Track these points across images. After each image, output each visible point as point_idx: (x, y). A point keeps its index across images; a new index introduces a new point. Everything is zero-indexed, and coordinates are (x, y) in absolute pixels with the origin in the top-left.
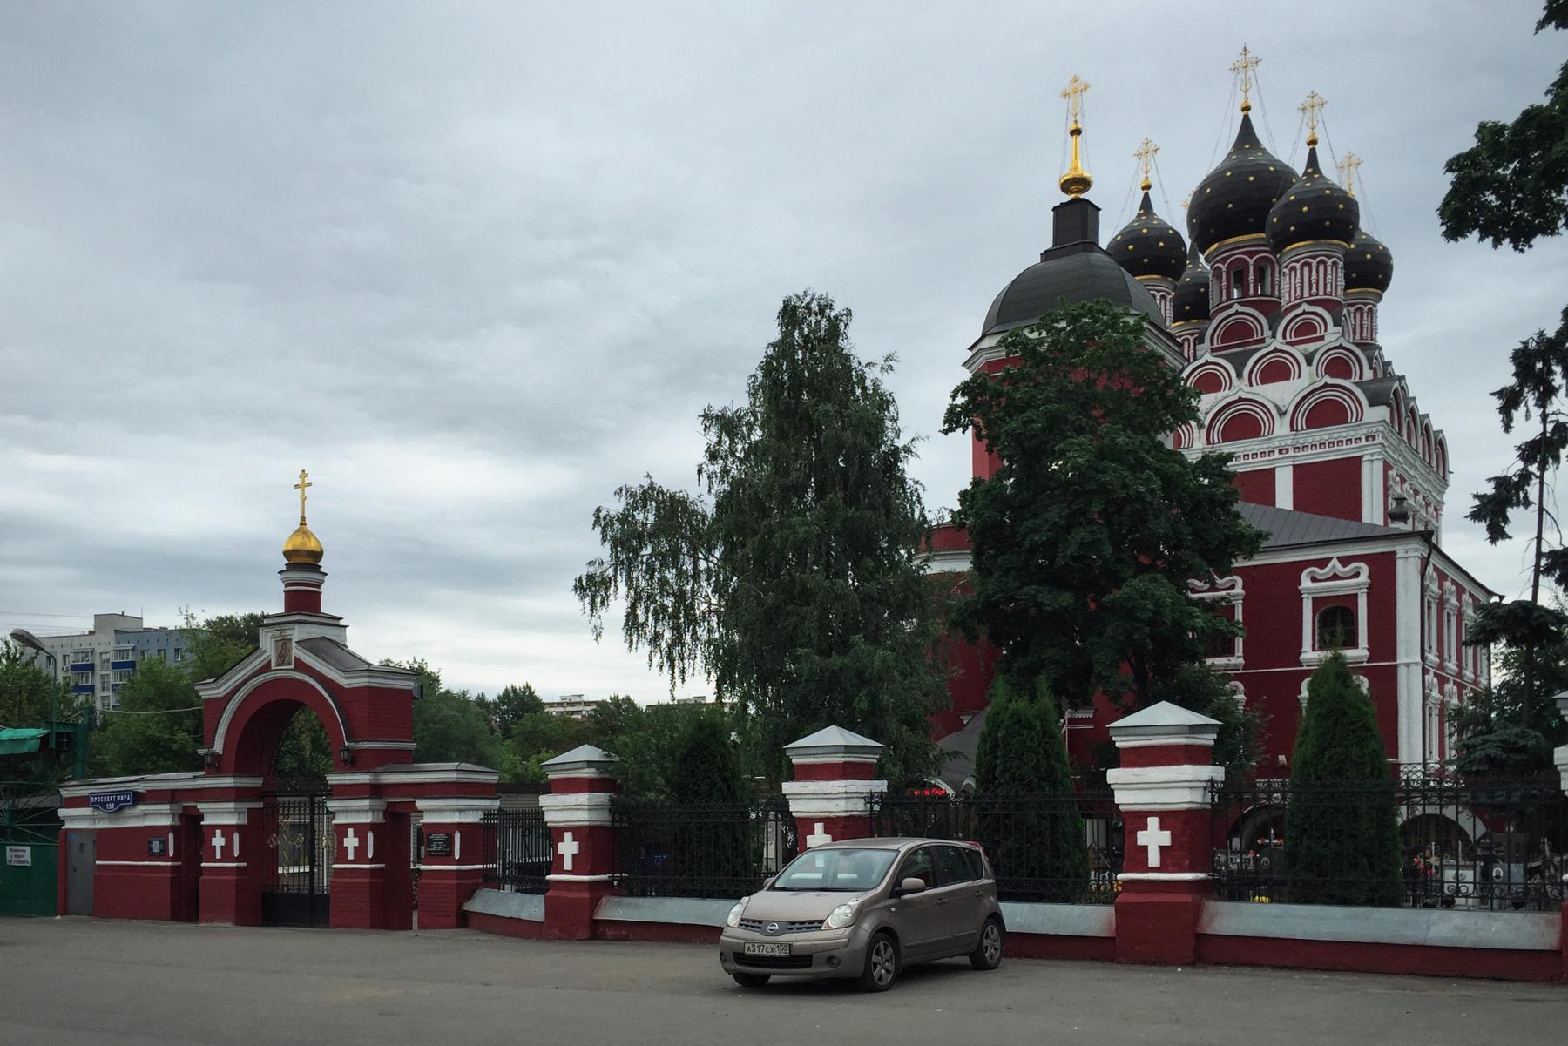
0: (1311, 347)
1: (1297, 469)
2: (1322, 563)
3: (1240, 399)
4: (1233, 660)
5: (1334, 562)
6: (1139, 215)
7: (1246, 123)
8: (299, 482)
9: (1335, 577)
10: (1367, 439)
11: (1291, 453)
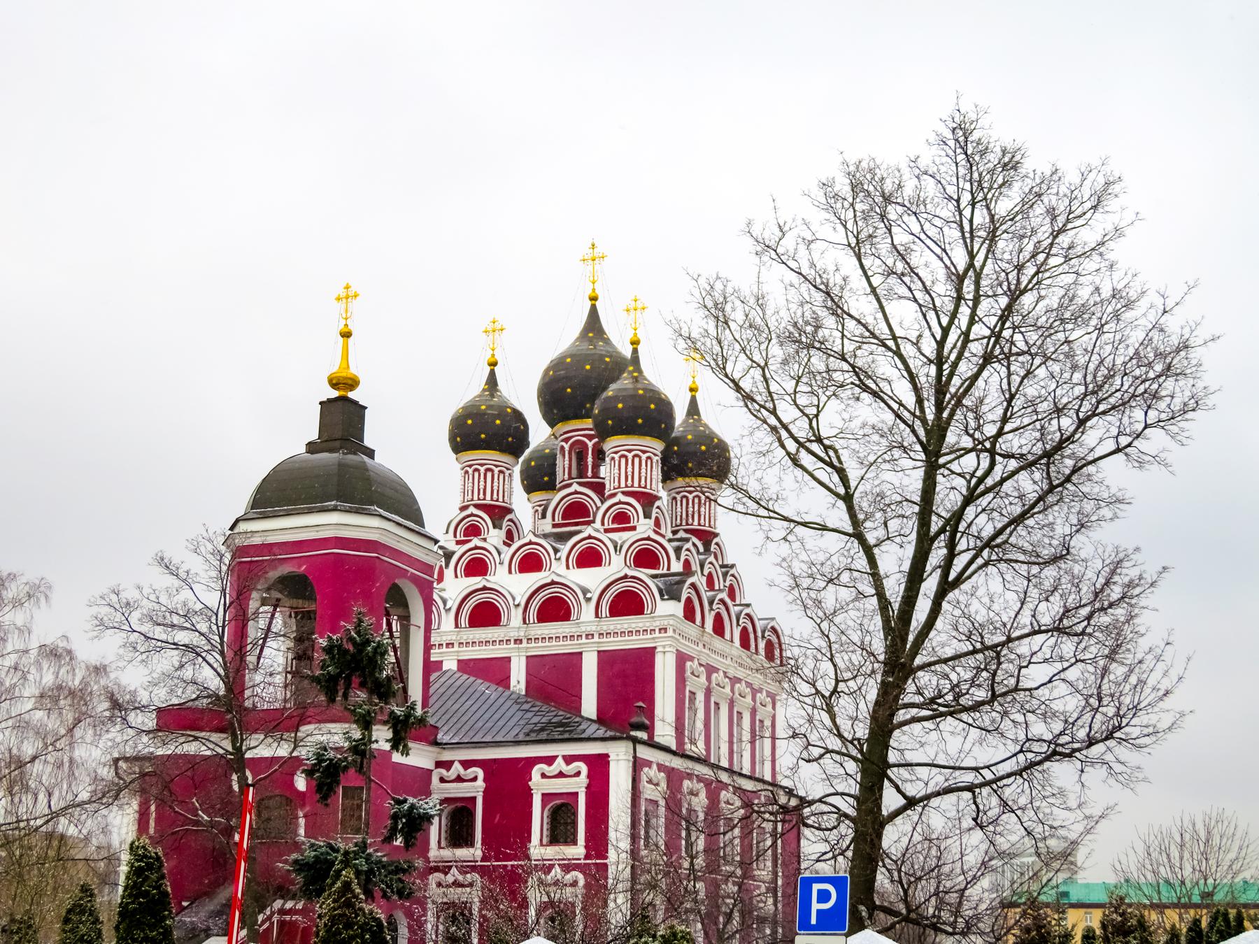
1: (600, 653)
2: (550, 760)
3: (553, 583)
5: (560, 761)
6: (484, 390)
7: (594, 313)
8: (343, 293)
9: (561, 775)
11: (596, 639)
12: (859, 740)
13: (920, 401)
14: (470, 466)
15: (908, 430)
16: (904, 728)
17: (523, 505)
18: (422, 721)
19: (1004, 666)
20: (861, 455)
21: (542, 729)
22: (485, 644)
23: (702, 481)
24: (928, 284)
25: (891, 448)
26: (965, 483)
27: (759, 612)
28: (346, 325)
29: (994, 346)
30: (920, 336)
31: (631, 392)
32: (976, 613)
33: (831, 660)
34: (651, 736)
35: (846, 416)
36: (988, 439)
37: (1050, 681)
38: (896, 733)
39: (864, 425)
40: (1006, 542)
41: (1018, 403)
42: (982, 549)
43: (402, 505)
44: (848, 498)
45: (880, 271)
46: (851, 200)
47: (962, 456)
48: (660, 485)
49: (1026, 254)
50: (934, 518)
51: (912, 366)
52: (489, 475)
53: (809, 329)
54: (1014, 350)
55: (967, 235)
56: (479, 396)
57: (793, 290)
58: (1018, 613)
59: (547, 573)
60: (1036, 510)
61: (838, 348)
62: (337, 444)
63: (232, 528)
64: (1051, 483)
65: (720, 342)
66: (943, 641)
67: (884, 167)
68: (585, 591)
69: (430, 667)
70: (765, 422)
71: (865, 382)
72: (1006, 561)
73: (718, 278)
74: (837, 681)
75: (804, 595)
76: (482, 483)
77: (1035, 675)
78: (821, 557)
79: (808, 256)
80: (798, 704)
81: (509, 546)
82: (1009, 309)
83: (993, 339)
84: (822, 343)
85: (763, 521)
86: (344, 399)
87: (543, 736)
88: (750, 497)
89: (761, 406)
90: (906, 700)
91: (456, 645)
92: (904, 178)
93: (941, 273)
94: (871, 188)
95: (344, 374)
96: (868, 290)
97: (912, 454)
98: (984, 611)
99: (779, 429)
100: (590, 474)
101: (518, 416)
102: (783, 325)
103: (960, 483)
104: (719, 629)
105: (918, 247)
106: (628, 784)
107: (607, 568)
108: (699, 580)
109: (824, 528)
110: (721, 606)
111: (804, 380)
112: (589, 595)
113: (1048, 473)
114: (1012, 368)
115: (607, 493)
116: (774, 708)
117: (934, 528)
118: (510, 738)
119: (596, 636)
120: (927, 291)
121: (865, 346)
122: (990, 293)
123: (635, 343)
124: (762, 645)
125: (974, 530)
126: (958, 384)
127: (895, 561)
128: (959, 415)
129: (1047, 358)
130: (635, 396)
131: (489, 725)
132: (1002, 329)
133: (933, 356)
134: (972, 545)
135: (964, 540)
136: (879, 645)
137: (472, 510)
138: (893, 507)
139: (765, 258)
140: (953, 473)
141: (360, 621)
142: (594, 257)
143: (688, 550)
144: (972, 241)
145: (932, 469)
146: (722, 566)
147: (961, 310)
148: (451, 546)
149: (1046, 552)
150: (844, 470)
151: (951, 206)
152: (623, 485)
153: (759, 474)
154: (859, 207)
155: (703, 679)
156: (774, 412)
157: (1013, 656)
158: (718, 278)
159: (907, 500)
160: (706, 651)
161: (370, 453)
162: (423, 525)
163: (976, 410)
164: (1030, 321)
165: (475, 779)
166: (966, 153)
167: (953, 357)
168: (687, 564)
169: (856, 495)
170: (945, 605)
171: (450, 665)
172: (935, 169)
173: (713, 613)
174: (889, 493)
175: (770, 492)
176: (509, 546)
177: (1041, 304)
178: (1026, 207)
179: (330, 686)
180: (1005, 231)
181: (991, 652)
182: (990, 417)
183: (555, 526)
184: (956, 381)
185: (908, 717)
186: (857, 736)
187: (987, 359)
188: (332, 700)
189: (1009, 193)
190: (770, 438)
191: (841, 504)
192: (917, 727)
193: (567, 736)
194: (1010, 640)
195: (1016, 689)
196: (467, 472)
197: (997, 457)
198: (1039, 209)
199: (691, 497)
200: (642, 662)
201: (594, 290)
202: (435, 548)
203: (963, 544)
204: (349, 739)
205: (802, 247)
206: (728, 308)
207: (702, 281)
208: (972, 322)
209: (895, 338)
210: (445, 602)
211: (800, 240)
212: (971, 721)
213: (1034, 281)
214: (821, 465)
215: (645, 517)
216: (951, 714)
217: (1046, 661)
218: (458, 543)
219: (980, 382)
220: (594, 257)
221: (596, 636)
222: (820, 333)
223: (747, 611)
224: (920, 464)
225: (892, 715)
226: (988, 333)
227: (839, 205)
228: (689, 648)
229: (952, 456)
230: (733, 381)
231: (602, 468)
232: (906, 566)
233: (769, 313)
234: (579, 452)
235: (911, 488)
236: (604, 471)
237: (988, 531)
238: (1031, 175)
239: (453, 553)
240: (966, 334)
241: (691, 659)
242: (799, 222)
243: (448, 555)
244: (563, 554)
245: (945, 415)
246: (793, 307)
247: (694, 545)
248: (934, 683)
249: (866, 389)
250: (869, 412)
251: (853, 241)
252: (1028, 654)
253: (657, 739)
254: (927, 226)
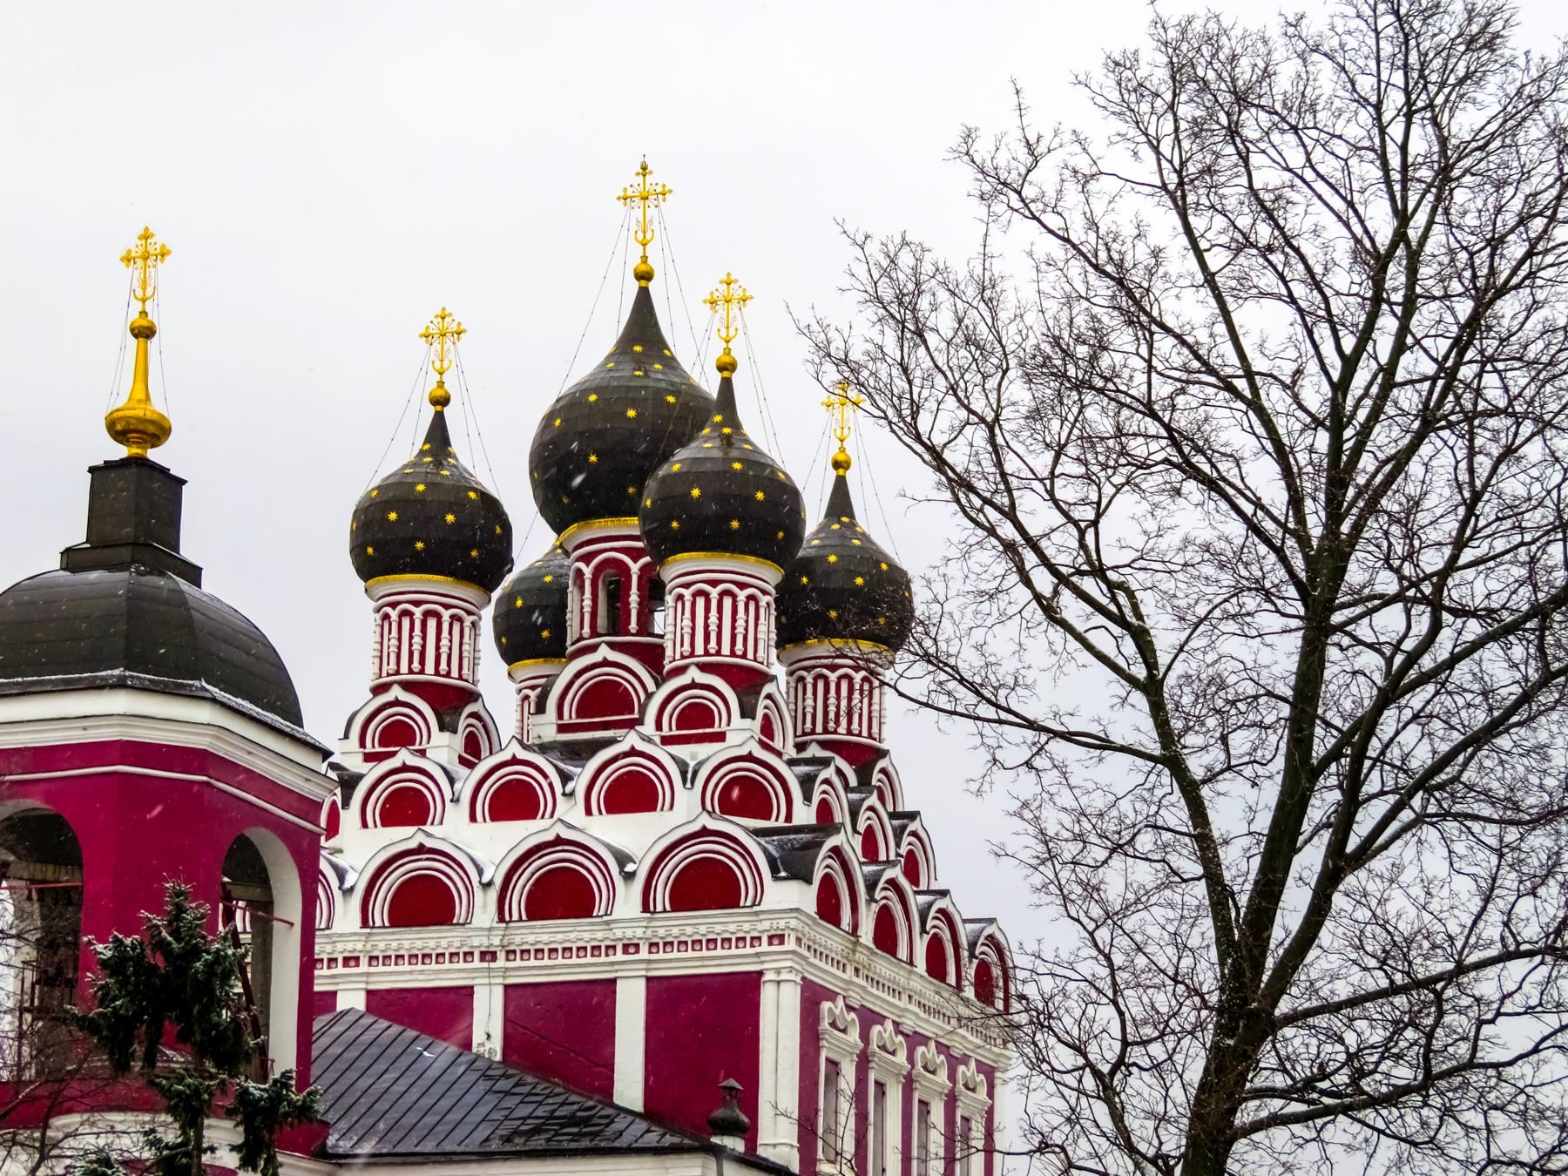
0: (703, 750)
3: (558, 841)
6: (422, 453)
7: (644, 303)
8: (136, 247)
10: (626, 948)
11: (644, 953)
12: (1165, 1158)
13: (1296, 502)
14: (393, 605)
15: (1272, 557)
16: (1257, 1136)
17: (498, 686)
18: (305, 1110)
19: (1447, 1019)
20: (1183, 603)
21: (537, 1130)
22: (420, 960)
23: (866, 646)
24: (1318, 269)
25: (1238, 591)
26: (1382, 663)
27: (966, 905)
28: (144, 313)
29: (1443, 396)
30: (1298, 372)
31: (719, 467)
32: (1399, 916)
33: (1115, 1003)
34: (752, 1143)
35: (1151, 526)
36: (1428, 577)
37: (1536, 1050)
38: (1240, 1146)
39: (1187, 542)
40: (1456, 779)
41: (1488, 509)
42: (1411, 793)
43: (260, 681)
44: (1152, 687)
45: (1224, 239)
46: (1168, 97)
47: (1376, 609)
48: (774, 652)
49: (1510, 218)
50: (1319, 731)
51: (1281, 431)
52: (432, 623)
53: (1082, 351)
54: (1482, 405)
55: (1396, 176)
56: (412, 465)
57: (1052, 274)
58: (1478, 917)
59: (547, 822)
60: (1515, 719)
61: (1139, 390)
62: (125, 553)
64: (1547, 665)
65: (905, 370)
66: (1333, 968)
67: (1237, 32)
68: (623, 859)
69: (313, 1004)
70: (991, 531)
71: (1192, 461)
72: (1456, 817)
73: (905, 243)
74: (1125, 1044)
75: (1065, 874)
76: (417, 640)
77: (1509, 1037)
78: (1099, 802)
79: (1082, 207)
80: (1050, 1085)
81: (471, 766)
82: (1473, 327)
83: (1440, 383)
84: (1107, 380)
85: (987, 729)
86: (139, 463)
87: (538, 1142)
88: (962, 681)
89: (986, 501)
90: (1259, 1082)
91: (364, 961)
92: (1276, 57)
93: (1343, 249)
94: (1211, 75)
95: (139, 413)
96: (1200, 278)
97: (1280, 603)
98: (1412, 912)
99: (1019, 550)
100: (633, 626)
101: (491, 508)
102: (1032, 341)
103: (1371, 662)
104: (886, 938)
105: (1299, 196)
107: (666, 814)
108: (848, 841)
109: (1105, 744)
111: (1072, 450)
112: (630, 868)
113: (1541, 648)
114: (1478, 442)
115: (668, 667)
116: (991, 1094)
117: (1319, 750)
118: (472, 1145)
119: (644, 949)
120: (1317, 285)
121: (1193, 389)
122: (1437, 292)
123: (727, 367)
124: (970, 972)
125: (1394, 754)
126: (1371, 469)
127: (1241, 811)
128: (1373, 529)
129: (1543, 425)
130: (726, 474)
131: (430, 1120)
132: (1459, 363)
133: (1323, 411)
134: (1390, 783)
135: (1375, 774)
136: (1208, 978)
137: (396, 692)
138: (1242, 706)
139: (999, 208)
140: (1360, 642)
141: (180, 909)
142: (645, 193)
143: (827, 781)
144: (1405, 189)
145: (1317, 634)
146: (894, 815)
147: (1380, 322)
148: (355, 764)
149: (1531, 801)
150: (1146, 632)
151: (1365, 116)
152: (700, 650)
153: (978, 636)
154: (1182, 110)
155: (854, 1036)
156: (1010, 514)
157: (1465, 1001)
158: (905, 243)
159: (1269, 694)
160: (861, 981)
161: (193, 574)
162: (298, 721)
163: (1405, 519)
164: (1513, 348)
166: (1396, 13)
167: (1362, 415)
168: (824, 810)
169: (1171, 680)
170: (1338, 900)
171: (351, 1000)
172: (1335, 43)
173: (875, 907)
174: (1231, 680)
175: (1001, 671)
176: (471, 766)
177: (1537, 316)
178: (1510, 123)
179: (116, 1037)
180: (1467, 171)
181: (1422, 989)
182: (1433, 535)
183: (562, 729)
184: (1367, 463)
185: (1264, 1114)
186: (1165, 1149)
187: (1429, 421)
188: (121, 1066)
189: (1479, 96)
190: (1003, 566)
191: (1139, 698)
192: (1280, 1135)
193: (585, 1143)
194: (1461, 969)
195: (1471, 1064)
196: (386, 617)
197: (1446, 616)
198: (1535, 130)
199: (833, 677)
200: (737, 997)
201: (644, 259)
202: (323, 768)
203: (1372, 785)
204: (155, 1143)
205: (1072, 189)
206: (924, 303)
207: (873, 248)
208: (1399, 348)
209: (1249, 375)
210: (341, 874)
211: (1067, 174)
212: (1380, 1124)
213: (1522, 273)
214: (1100, 620)
215: (743, 715)
216: (1345, 1110)
217: (1529, 1010)
218: (369, 758)
219: (1415, 467)
220: (645, 193)
221: (644, 949)
222: (1105, 361)
223: (941, 903)
224: (1295, 623)
225: (1233, 1111)
226: (1430, 368)
227: (1145, 107)
228: (827, 975)
229: (1359, 610)
230: (931, 449)
231: (658, 617)
232: (1264, 822)
233: (1004, 316)
234: (613, 580)
235: (1276, 670)
236: (660, 621)
237: (1422, 758)
238: (1521, 62)
239: (360, 777)
240: (1389, 370)
241: (831, 996)
242: (1067, 137)
243: (348, 782)
244: (579, 785)
245: (1345, 528)
246: (1052, 306)
247: (839, 772)
248: (1313, 1050)
249: (1193, 472)
250: (1195, 518)
251: (1172, 179)
252: (1498, 996)
253: (762, 1152)
254: (1318, 154)
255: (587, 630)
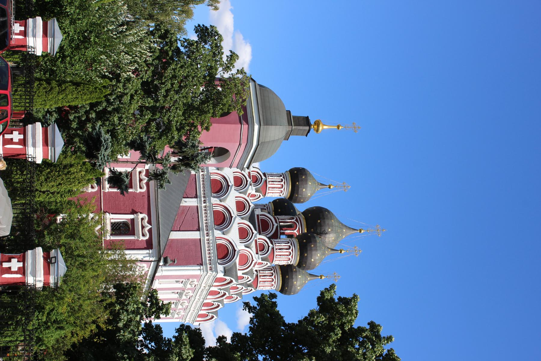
0: (254, 249)
2: (149, 222)
3: (232, 217)
4: (108, 235)
5: (150, 227)
9: (143, 227)
11: (203, 205)
63: (252, 79)
106: (155, 203)
110: (223, 294)
165: (141, 188)
176: (248, 196)
183: (258, 215)
218: (249, 173)
255: (280, 220)
